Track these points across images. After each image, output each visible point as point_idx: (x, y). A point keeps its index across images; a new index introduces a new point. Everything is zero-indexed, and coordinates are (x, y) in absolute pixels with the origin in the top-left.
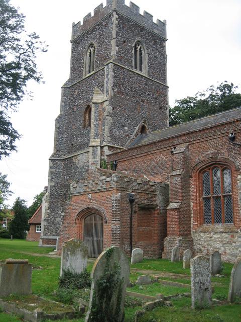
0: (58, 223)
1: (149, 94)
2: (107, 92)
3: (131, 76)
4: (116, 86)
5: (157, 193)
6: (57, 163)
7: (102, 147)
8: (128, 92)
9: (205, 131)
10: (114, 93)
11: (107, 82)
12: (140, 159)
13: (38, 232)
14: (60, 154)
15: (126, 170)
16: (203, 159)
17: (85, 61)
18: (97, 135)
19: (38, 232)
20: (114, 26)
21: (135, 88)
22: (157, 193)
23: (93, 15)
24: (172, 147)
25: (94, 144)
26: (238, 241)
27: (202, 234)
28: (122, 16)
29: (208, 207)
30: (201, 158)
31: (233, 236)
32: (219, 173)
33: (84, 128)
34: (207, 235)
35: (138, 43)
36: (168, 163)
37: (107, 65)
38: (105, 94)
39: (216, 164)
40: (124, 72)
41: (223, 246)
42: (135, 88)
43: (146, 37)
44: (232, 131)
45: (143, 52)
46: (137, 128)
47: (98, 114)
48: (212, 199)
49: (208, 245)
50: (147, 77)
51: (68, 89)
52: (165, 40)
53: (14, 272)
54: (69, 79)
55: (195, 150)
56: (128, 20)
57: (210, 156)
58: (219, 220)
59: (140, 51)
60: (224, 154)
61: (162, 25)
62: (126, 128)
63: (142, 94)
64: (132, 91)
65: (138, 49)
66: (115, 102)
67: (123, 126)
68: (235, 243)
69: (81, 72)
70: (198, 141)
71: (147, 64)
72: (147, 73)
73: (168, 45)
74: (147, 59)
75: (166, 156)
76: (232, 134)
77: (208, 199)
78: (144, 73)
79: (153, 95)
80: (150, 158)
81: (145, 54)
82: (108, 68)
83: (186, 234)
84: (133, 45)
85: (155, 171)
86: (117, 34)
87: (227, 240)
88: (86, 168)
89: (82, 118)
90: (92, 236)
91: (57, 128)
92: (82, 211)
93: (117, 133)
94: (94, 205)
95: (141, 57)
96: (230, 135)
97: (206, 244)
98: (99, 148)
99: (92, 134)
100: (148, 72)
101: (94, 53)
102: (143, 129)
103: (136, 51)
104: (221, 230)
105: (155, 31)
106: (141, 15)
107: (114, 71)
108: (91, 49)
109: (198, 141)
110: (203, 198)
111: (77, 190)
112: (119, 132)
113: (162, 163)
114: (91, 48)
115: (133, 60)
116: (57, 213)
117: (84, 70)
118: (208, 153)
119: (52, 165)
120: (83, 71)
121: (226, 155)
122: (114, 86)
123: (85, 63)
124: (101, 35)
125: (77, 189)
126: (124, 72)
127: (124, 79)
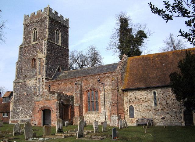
0: (19, 112)
2: (44, 53)
7: (42, 79)
11: (44, 49)
16: (88, 87)
17: (32, 36)
18: (40, 73)
20: (48, 23)
23: (36, 14)
27: (87, 115)
28: (51, 18)
29: (89, 105)
31: (98, 115)
35: (57, 30)
37: (45, 41)
43: (58, 26)
46: (57, 70)
47: (40, 64)
48: (91, 102)
52: (68, 28)
54: (23, 43)
56: (54, 19)
59: (58, 34)
61: (67, 20)
66: (48, 58)
73: (69, 30)
77: (90, 102)
82: (45, 42)
83: (81, 115)
84: (55, 31)
86: (49, 26)
89: (31, 64)
91: (17, 67)
95: (58, 36)
98: (41, 79)
100: (61, 43)
101: (37, 32)
103: (56, 34)
105: (64, 24)
106: (59, 17)
107: (48, 44)
108: (35, 31)
111: (38, 99)
117: (31, 40)
120: (31, 41)
121: (96, 86)
123: (31, 37)
124: (41, 25)
127: (51, 47)
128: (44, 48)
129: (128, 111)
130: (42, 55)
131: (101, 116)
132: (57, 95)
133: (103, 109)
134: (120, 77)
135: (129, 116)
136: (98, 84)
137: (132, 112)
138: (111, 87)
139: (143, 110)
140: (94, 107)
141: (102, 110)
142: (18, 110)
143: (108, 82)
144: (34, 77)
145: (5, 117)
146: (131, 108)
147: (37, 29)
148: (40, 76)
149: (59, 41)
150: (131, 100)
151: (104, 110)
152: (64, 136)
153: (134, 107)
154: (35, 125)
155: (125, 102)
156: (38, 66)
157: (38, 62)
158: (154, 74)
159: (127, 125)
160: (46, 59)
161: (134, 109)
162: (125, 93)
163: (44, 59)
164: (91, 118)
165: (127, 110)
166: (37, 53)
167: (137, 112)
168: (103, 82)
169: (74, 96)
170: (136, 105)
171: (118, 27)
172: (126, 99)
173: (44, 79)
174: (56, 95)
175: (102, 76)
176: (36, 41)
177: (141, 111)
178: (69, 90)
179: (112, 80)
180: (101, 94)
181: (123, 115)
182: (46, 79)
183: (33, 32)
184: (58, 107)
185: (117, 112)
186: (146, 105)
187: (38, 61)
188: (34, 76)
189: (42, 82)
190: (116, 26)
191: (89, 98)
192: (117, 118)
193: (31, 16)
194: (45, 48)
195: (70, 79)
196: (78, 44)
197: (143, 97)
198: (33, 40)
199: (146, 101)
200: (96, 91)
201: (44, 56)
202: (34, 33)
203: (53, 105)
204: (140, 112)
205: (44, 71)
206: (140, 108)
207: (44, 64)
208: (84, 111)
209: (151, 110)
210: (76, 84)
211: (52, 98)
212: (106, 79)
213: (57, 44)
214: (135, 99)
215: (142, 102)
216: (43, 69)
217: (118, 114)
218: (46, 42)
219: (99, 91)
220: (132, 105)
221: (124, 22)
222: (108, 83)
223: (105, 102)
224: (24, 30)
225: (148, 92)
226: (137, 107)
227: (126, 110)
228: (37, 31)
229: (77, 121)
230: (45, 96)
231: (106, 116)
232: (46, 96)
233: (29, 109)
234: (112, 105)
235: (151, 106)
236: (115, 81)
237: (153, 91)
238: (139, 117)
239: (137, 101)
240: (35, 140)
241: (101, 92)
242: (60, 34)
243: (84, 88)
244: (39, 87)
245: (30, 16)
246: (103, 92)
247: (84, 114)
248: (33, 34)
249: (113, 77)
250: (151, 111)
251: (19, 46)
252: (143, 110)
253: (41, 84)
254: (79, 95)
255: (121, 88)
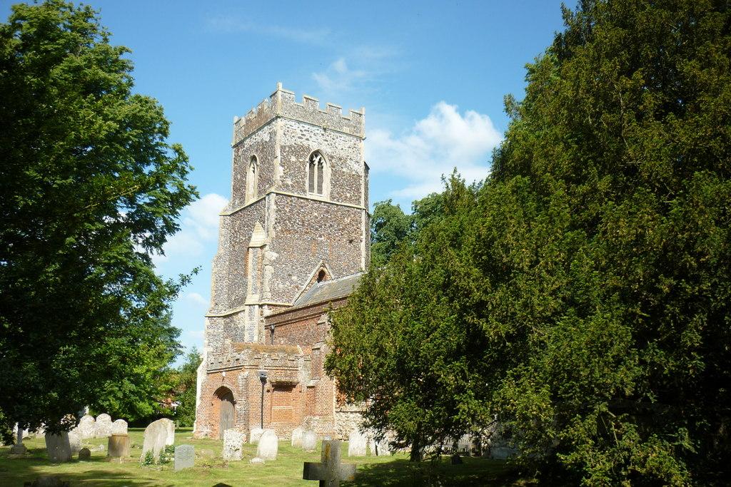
1: (331, 226)
3: (303, 205)
4: (279, 223)
5: (299, 369)
10: (277, 232)
14: (220, 308)
22: (299, 369)
32: (16, 429)
45: (324, 164)
51: (229, 217)
53: (256, 479)
62: (294, 278)
65: (316, 163)
67: (290, 275)
69: (242, 197)
78: (325, 196)
93: (281, 286)
99: (250, 288)
102: (321, 276)
122: (276, 223)
126: (291, 201)
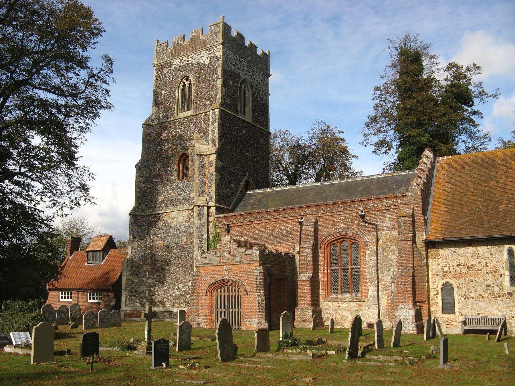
2: (213, 142)
3: (236, 123)
6: (139, 219)
7: (209, 208)
8: (234, 142)
9: (335, 205)
12: (260, 226)
13: (63, 300)
15: (242, 236)
16: (332, 233)
17: (176, 96)
19: (63, 300)
21: (240, 137)
24: (298, 217)
25: (199, 203)
26: (365, 310)
29: (336, 278)
30: (331, 231)
31: (360, 305)
33: (179, 179)
34: (335, 304)
36: (295, 233)
38: (211, 145)
39: (345, 238)
40: (230, 118)
41: (351, 315)
42: (240, 137)
44: (362, 209)
45: (247, 91)
47: (202, 168)
48: (339, 271)
49: (336, 313)
50: (251, 122)
54: (153, 114)
55: (324, 222)
57: (340, 230)
58: (345, 291)
60: (353, 231)
61: (266, 57)
63: (247, 144)
64: (237, 140)
66: (220, 154)
68: (362, 311)
70: (328, 214)
71: (251, 107)
72: (251, 119)
74: (251, 101)
75: (291, 225)
76: (362, 212)
79: (257, 144)
80: (272, 226)
81: (249, 94)
83: (315, 302)
84: (239, 85)
85: (278, 240)
87: (355, 309)
88: (184, 229)
90: (226, 307)
92: (215, 283)
93: (224, 191)
94: (229, 276)
96: (360, 212)
97: (334, 312)
98: (206, 208)
100: (252, 116)
103: (240, 91)
104: (350, 300)
106: (246, 47)
108: (186, 83)
109: (328, 214)
110: (331, 270)
111: (207, 260)
112: (226, 190)
113: (286, 233)
114: (185, 81)
115: (239, 103)
116: (142, 280)
118: (338, 227)
119: (133, 221)
121: (356, 231)
123: (176, 98)
125: (207, 259)
128: (211, 127)
129: (440, 296)
130: (205, 146)
131: (367, 308)
132: (258, 253)
133: (372, 290)
134: (419, 209)
135: (441, 309)
136: (359, 226)
137: (447, 297)
138: (395, 233)
139: (480, 295)
140: (349, 282)
141: (370, 292)
142: (141, 285)
143: (386, 221)
144: (185, 203)
145: (67, 300)
146: (447, 290)
147: (191, 78)
148: (201, 201)
149: (247, 109)
150: (446, 269)
151: (376, 293)
152: (313, 354)
153: (455, 285)
154: (199, 324)
155: (430, 274)
156: (196, 175)
157: (194, 165)
158: (508, 204)
159: (441, 332)
160: (218, 159)
161: (455, 290)
162: (431, 252)
163: (213, 157)
164: (47, 285)
165: (436, 293)
166: (193, 139)
167: (463, 299)
168: (373, 221)
169: (294, 253)
170: (462, 280)
171: (393, 75)
172: (434, 266)
173: (213, 210)
174: (255, 252)
175: (370, 204)
176: (189, 109)
177: (472, 298)
178: (281, 237)
179: (399, 217)
180: (368, 252)
181: (425, 306)
182: (219, 210)
183: (181, 87)
184: (261, 282)
185: (411, 298)
186: (488, 283)
187: (197, 162)
188: (184, 201)
189: (208, 216)
190: (383, 69)
191: (332, 260)
192: (412, 313)
193: (174, 45)
194: (215, 128)
195: (284, 210)
196: (292, 116)
197: (479, 260)
198: (180, 107)
199: (488, 273)
200: (354, 243)
201: (211, 148)
202: (183, 90)
203: (250, 275)
204: (471, 300)
205: (214, 188)
206: (472, 290)
207: (213, 169)
208: (322, 293)
209: (499, 296)
210: (300, 223)
211: (244, 259)
212: (382, 213)
213: (243, 118)
214: (458, 265)
215: (476, 276)
216: (211, 183)
217: (415, 303)
218: (217, 113)
219: (362, 244)
220: (451, 281)
221: (410, 61)
222: (388, 224)
223: (378, 270)
224: (156, 80)
225: (493, 249)
226: (463, 286)
227: (432, 293)
228: (190, 84)
229: (304, 315)
230: (226, 254)
231: (381, 308)
232: (230, 253)
233: (171, 285)
234: (400, 279)
235: (500, 286)
236: (407, 219)
237: (507, 247)
238: (472, 314)
239: (464, 270)
240: (255, 362)
241: (367, 246)
242: (251, 92)
243: (321, 237)
244: (200, 228)
245: (171, 45)
246: (373, 247)
247: (321, 300)
248: (180, 91)
249: (402, 208)
250: (500, 299)
251: (143, 121)
252: (480, 295)
253: (205, 220)
254: (309, 251)
255: (422, 237)
